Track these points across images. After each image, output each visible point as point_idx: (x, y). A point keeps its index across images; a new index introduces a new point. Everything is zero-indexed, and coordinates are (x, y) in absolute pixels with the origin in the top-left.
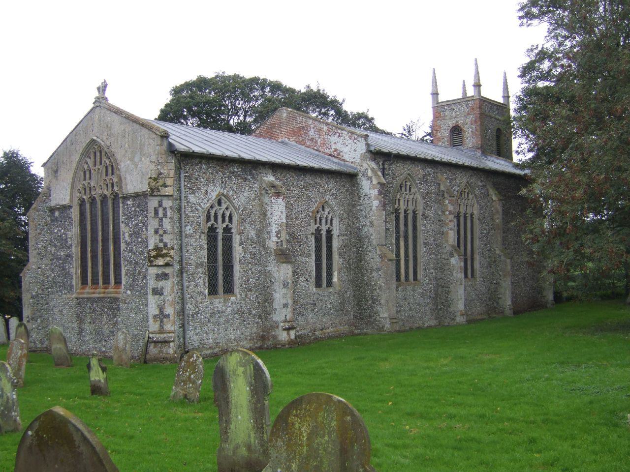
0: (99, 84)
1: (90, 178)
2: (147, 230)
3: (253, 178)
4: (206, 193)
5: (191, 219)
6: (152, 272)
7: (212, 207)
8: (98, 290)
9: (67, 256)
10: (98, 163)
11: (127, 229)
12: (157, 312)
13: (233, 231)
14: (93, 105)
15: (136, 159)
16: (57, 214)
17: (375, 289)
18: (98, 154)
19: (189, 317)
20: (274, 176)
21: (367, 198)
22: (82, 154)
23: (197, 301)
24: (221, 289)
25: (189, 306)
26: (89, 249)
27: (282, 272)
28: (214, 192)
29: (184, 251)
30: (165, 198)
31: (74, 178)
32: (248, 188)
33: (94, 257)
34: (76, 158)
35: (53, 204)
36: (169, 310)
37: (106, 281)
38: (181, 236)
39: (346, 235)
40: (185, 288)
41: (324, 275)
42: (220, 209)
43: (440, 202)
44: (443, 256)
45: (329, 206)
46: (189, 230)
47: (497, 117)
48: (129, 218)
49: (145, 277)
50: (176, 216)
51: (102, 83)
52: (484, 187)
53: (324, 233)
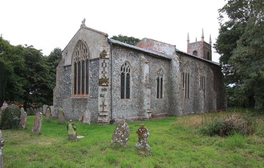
0: (82, 20)
1: (78, 55)
2: (99, 72)
3: (138, 56)
4: (121, 60)
5: (115, 70)
6: (100, 88)
7: (123, 66)
8: (80, 96)
9: (70, 83)
10: (81, 49)
11: (91, 73)
12: (102, 104)
13: (130, 75)
14: (80, 28)
15: (95, 46)
16: (67, 68)
17: (177, 100)
18: (81, 46)
19: (113, 107)
20: (145, 57)
21: (175, 68)
22: (76, 46)
23: (117, 101)
24: (125, 97)
25: (113, 102)
26: (77, 81)
27: (148, 91)
28: (124, 60)
29: (113, 81)
30: (106, 59)
31: (73, 55)
32: (136, 60)
33: (79, 84)
34: (73, 47)
35: (65, 65)
36: (106, 103)
37: (83, 93)
38: (112, 75)
39: (167, 80)
40: (112, 96)
41: (160, 94)
42: (126, 67)
43: (196, 72)
44: (197, 90)
45: (162, 70)
46: (114, 73)
47: (208, 48)
48: (92, 68)
49: (97, 91)
50: (110, 67)
51: (84, 20)
52: (208, 68)
53: (160, 79)
